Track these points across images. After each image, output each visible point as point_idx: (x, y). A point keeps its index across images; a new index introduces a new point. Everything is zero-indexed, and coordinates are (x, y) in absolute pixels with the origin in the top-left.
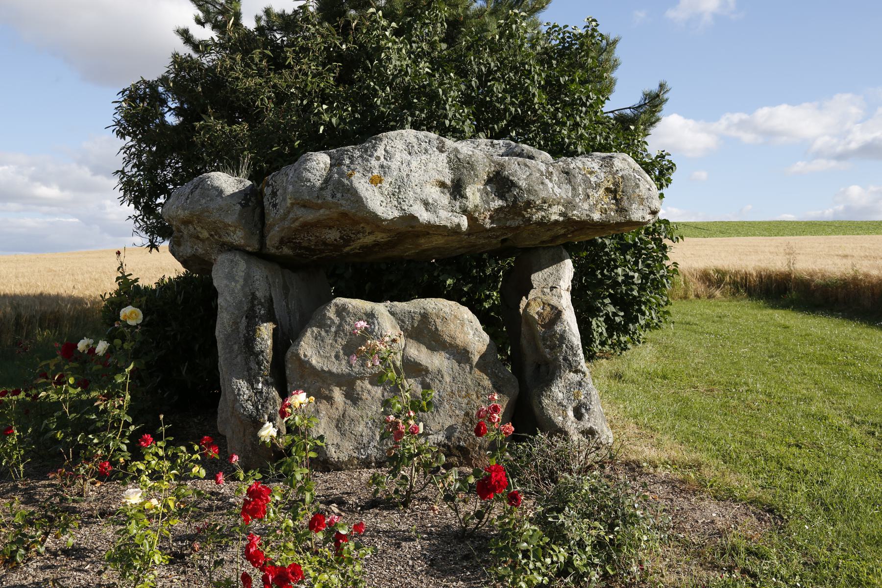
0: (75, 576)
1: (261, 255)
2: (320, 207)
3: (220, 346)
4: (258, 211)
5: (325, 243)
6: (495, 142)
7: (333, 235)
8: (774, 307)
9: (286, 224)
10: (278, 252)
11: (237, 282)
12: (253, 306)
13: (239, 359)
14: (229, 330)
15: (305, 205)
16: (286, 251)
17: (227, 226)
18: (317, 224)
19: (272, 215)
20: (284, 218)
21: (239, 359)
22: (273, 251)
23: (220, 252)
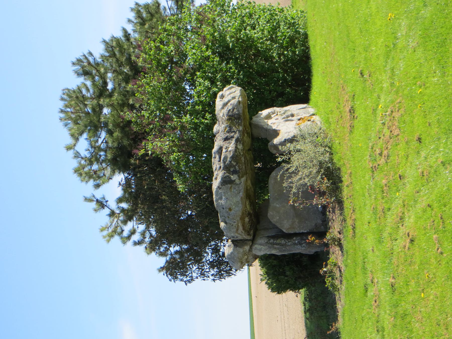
0: (449, 227)
1: (253, 241)
2: (238, 226)
3: (283, 253)
4: (239, 241)
5: (249, 221)
6: (213, 156)
7: (247, 220)
8: (264, 255)
9: (243, 234)
10: (252, 235)
11: (262, 248)
12: (270, 243)
13: (287, 248)
14: (278, 251)
15: (237, 230)
16: (252, 232)
17: (243, 251)
18: (243, 226)
19: (240, 238)
20: (242, 235)
21: (287, 248)
22: (252, 237)
23: (251, 251)
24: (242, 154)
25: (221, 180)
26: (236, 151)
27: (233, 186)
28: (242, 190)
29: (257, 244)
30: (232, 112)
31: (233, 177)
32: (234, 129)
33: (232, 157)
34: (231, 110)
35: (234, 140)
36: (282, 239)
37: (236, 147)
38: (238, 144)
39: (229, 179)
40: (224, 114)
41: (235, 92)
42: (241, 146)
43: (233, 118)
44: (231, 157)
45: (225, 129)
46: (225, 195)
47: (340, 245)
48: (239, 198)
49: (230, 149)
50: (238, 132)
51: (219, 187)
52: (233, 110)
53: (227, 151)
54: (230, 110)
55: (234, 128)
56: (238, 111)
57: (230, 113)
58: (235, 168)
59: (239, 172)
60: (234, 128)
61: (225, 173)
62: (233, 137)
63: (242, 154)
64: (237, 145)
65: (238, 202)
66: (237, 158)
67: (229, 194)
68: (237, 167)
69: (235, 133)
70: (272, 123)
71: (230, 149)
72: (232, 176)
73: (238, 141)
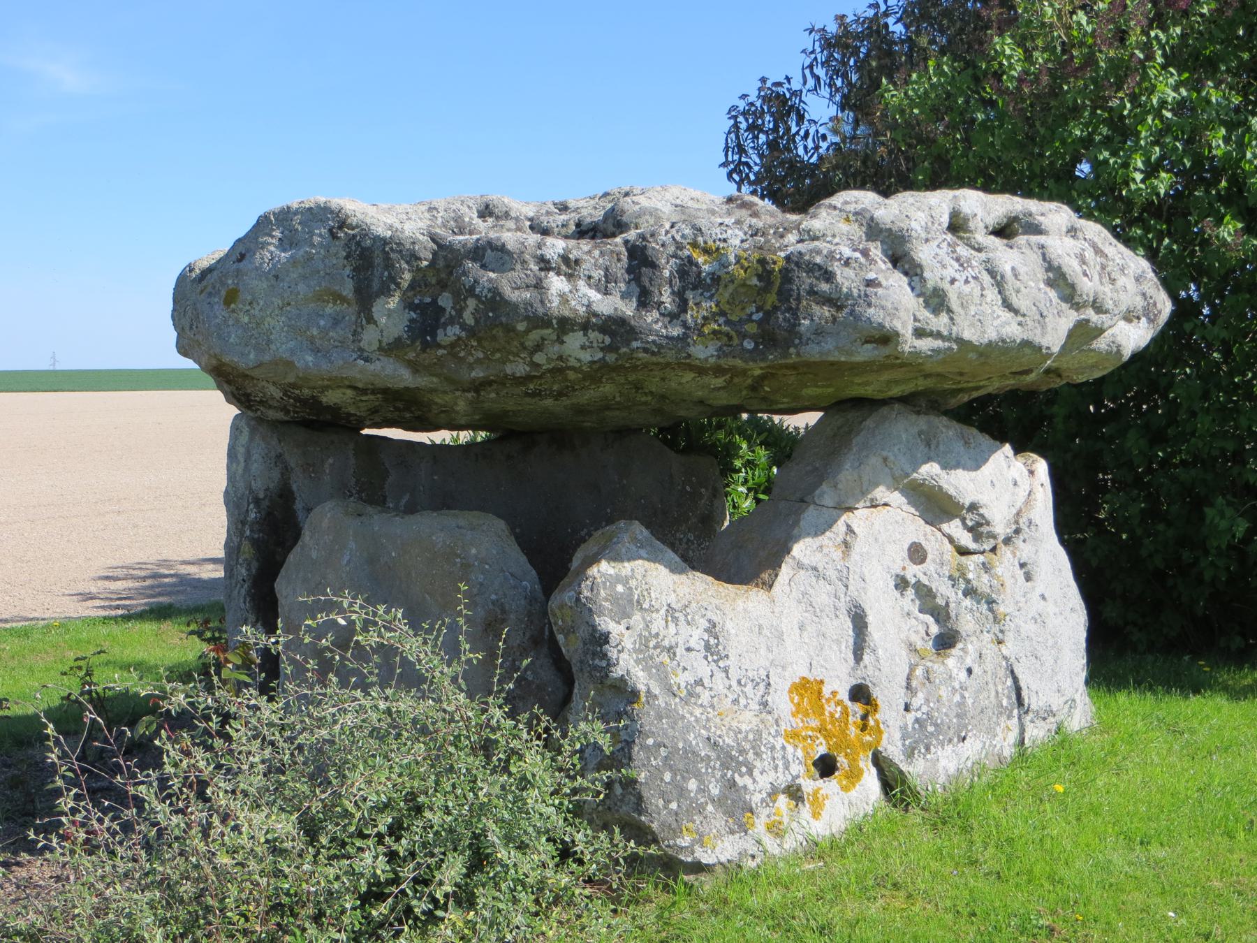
24: (539, 358)
25: (378, 239)
26: (542, 321)
27: (350, 312)
28: (325, 366)
29: (251, 439)
30: (812, 292)
31: (390, 312)
32: (701, 309)
33: (495, 301)
34: (824, 287)
35: (628, 309)
36: (255, 565)
37: (565, 325)
38: (593, 335)
39: (376, 285)
40: (815, 238)
41: (1007, 305)
42: (586, 357)
43: (772, 298)
44: (495, 291)
45: (706, 251)
46: (293, 261)
47: (913, 649)
48: (283, 347)
49: (557, 284)
50: (676, 331)
51: (343, 224)
52: (828, 300)
53: (545, 264)
54: (829, 276)
55: (709, 305)
56: (819, 332)
57: (804, 280)
58: (451, 321)
59: (426, 346)
60: (709, 305)
61: (413, 257)
62: (645, 300)
63: (539, 358)
64: (585, 327)
65: (269, 342)
66: (498, 332)
67: (302, 287)
68: (453, 332)
69: (672, 317)
70: (850, 530)
71: (557, 284)
72: (393, 302)
73: (612, 334)
